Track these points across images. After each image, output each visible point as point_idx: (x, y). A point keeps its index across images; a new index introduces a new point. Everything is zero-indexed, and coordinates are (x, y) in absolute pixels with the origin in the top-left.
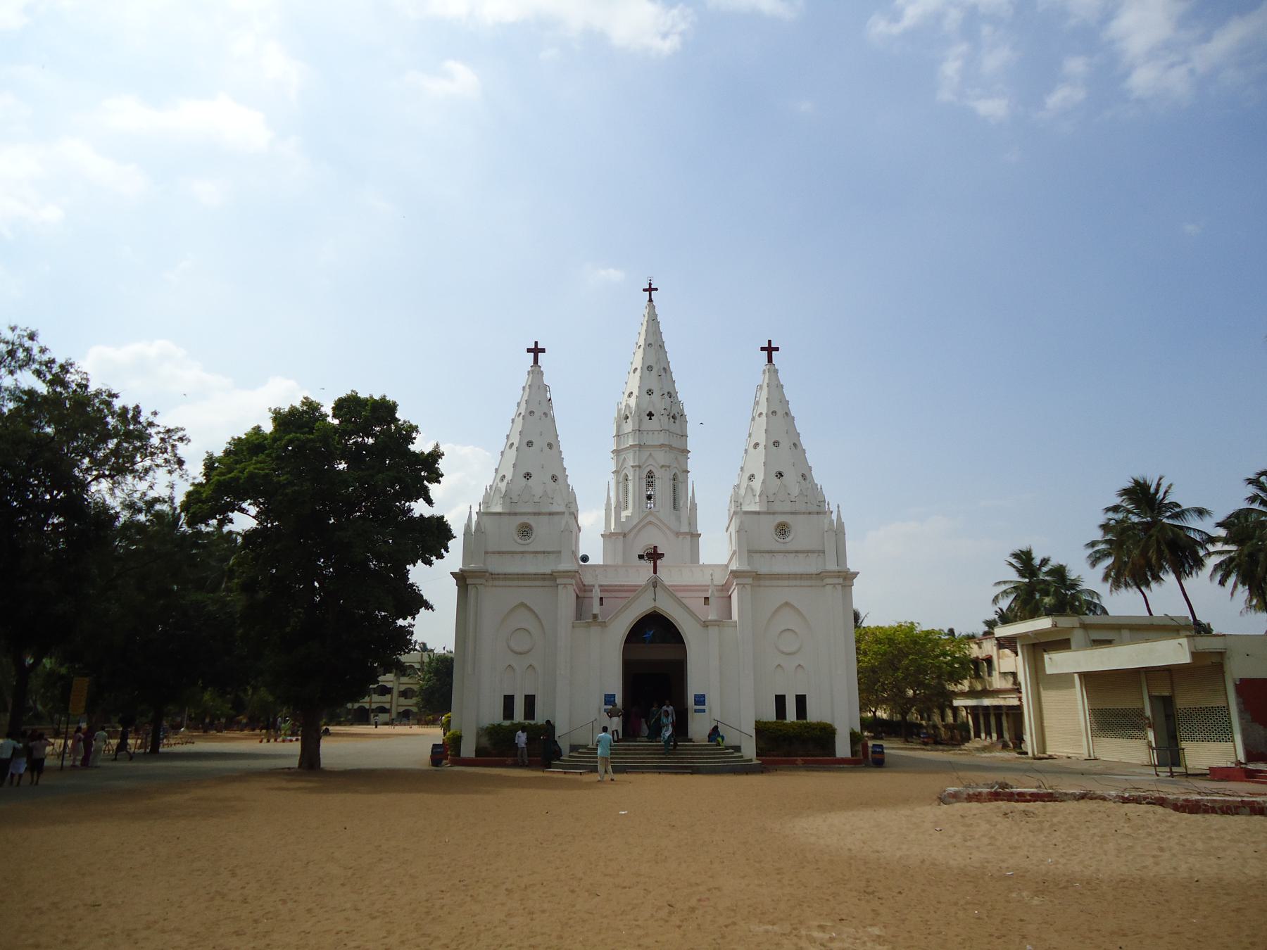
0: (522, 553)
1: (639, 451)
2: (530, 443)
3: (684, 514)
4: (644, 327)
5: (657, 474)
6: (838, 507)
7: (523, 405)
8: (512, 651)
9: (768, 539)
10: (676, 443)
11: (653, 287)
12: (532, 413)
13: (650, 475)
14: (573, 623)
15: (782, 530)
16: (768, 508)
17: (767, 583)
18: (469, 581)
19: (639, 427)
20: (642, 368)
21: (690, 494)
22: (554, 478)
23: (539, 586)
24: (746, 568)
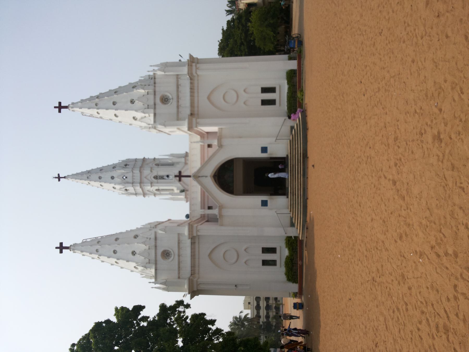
0: (179, 256)
1: (143, 183)
2: (115, 252)
3: (175, 160)
4: (79, 181)
5: (155, 174)
6: (151, 66)
7: (93, 256)
8: (236, 261)
9: (171, 108)
10: (139, 164)
11: (57, 176)
12: (97, 251)
13: (156, 177)
14: (220, 225)
15: (165, 100)
16: (151, 108)
17: (196, 109)
18: (195, 289)
19: (131, 183)
20: (100, 182)
21: (167, 157)
22: (136, 237)
23: (199, 246)
24: (186, 122)
